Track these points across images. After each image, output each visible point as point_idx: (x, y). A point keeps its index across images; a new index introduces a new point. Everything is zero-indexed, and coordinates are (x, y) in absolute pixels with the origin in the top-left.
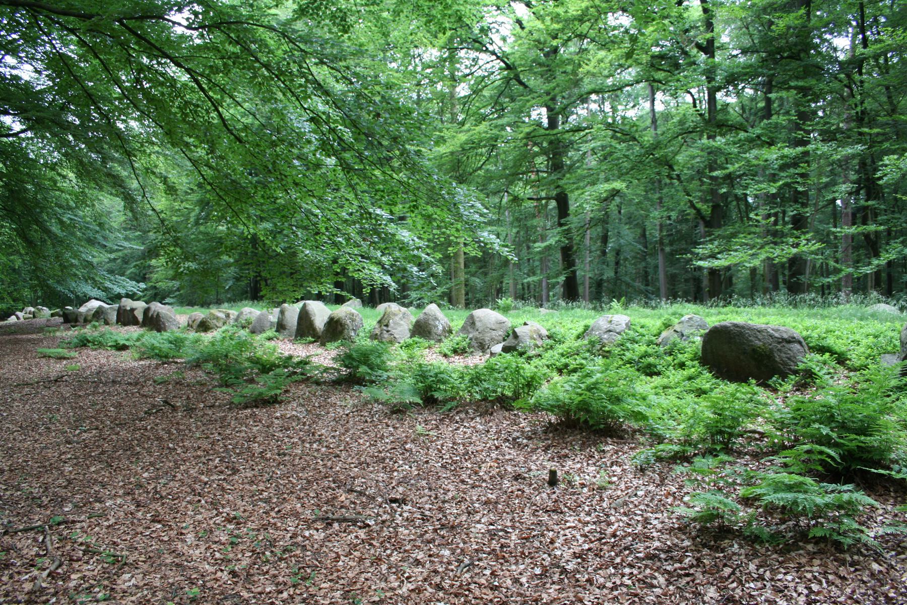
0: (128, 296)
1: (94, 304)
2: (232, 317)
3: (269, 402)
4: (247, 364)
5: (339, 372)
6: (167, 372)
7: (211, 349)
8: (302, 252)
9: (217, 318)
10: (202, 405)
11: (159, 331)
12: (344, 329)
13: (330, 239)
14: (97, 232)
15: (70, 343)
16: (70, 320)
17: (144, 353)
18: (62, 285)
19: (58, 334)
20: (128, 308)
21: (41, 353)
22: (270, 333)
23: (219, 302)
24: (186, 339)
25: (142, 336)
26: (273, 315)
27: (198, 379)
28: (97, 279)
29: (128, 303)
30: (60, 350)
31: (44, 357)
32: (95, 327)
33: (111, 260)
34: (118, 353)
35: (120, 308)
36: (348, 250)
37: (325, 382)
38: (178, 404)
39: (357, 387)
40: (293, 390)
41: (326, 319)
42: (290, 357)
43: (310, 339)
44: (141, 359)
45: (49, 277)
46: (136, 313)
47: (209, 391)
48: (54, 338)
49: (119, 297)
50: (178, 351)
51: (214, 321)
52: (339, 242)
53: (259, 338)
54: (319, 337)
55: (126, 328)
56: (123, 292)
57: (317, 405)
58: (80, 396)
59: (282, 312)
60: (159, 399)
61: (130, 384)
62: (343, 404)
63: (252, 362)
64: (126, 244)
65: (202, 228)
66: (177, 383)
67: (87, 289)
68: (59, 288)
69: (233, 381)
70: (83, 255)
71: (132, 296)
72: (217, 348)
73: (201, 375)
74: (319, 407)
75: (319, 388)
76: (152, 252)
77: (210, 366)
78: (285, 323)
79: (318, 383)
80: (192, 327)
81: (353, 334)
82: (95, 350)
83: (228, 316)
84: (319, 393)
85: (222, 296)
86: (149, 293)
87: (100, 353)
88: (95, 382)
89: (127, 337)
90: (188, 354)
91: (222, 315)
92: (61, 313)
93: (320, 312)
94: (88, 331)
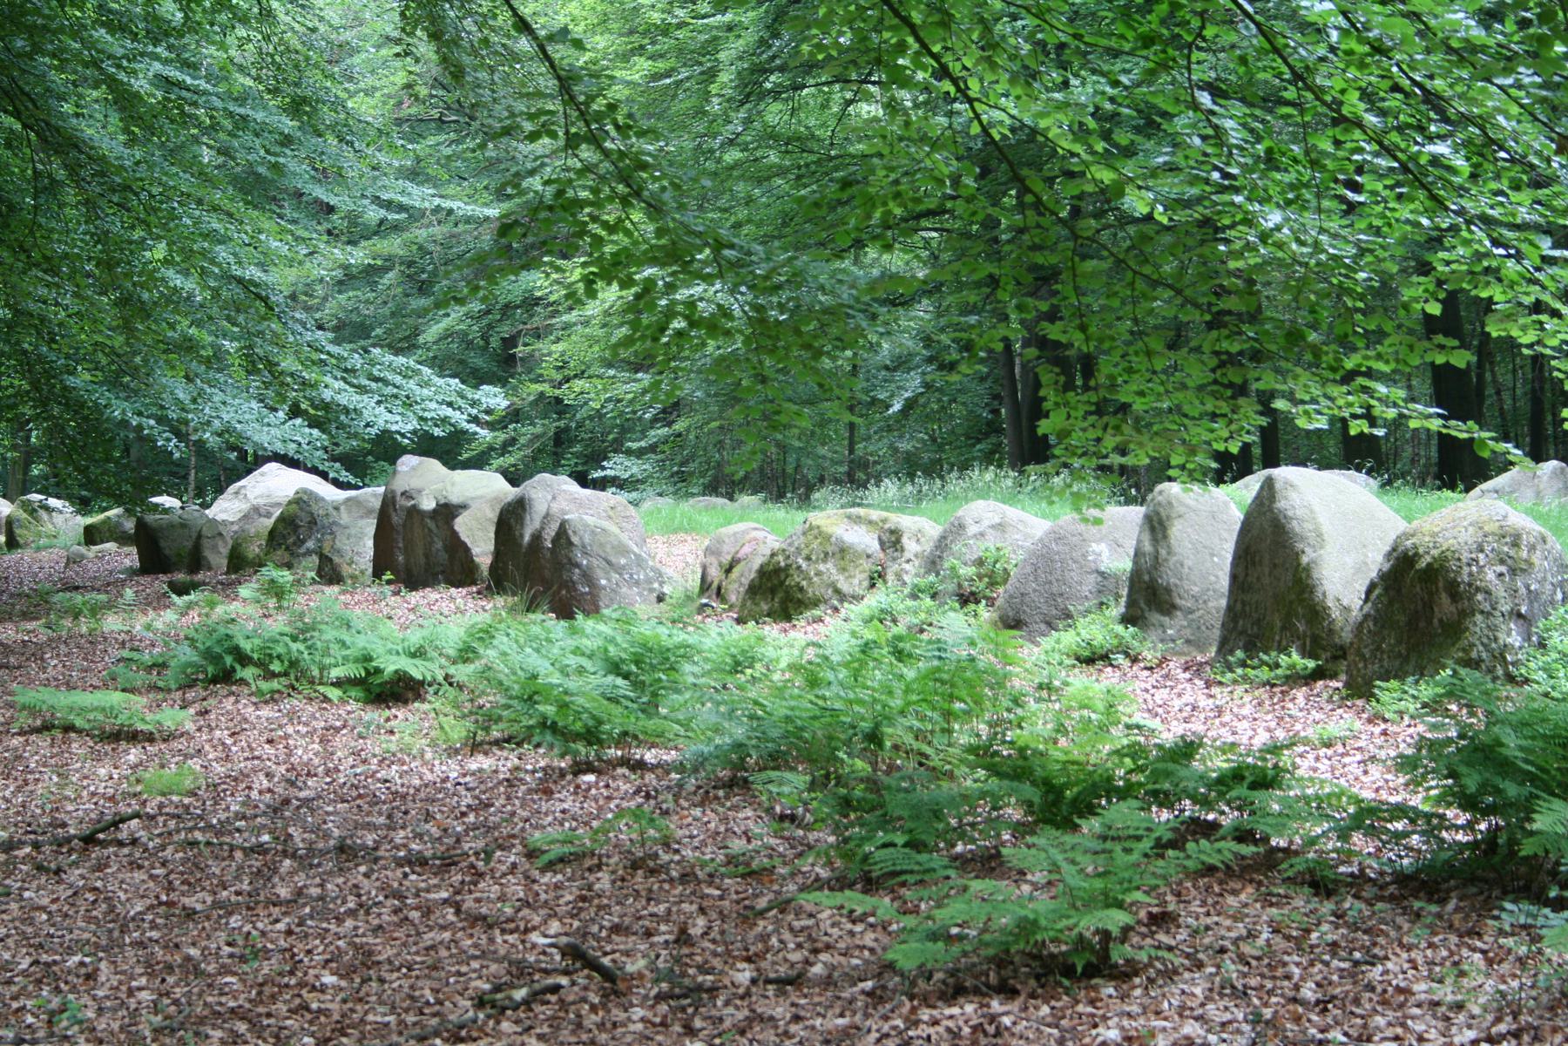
0: (427, 446)
1: (275, 485)
2: (911, 546)
3: (1069, 971)
4: (973, 780)
5: (1429, 833)
6: (596, 809)
7: (805, 704)
8: (1249, 222)
9: (843, 553)
10: (744, 975)
11: (565, 611)
12: (1466, 614)
13: (1388, 151)
14: (287, 141)
15: (161, 666)
16: (169, 558)
17: (491, 719)
18: (131, 394)
19: (112, 623)
20: (428, 504)
21: (33, 711)
22: (1100, 628)
23: (857, 476)
24: (687, 652)
25: (486, 634)
26: (1111, 537)
27: (738, 845)
28: (288, 363)
29: (426, 480)
30: (116, 698)
31: (46, 727)
32: (276, 591)
33: (349, 278)
34: (374, 715)
35: (388, 502)
36: (1479, 203)
37: (1360, 879)
38: (635, 966)
39: (1514, 912)
40: (1193, 913)
41: (1376, 561)
42: (1186, 750)
43: (1296, 659)
44: (475, 747)
45: (76, 358)
46: (462, 525)
47: (784, 906)
48: (95, 639)
49: (387, 449)
50: (649, 709)
51: (829, 567)
52: (1435, 161)
53: (1033, 657)
54: (1340, 653)
55: (415, 597)
56: (403, 425)
57: (1309, 992)
58: (190, 914)
59: (1156, 526)
60: (546, 936)
61: (418, 862)
62: (1446, 993)
63: (994, 770)
64: (419, 196)
65: (774, 113)
66: (635, 865)
67: (240, 412)
68: (119, 409)
69: (897, 857)
70: (222, 253)
71: (448, 448)
72: (833, 695)
73: (749, 828)
74: (1322, 1006)
75: (1328, 907)
76: (532, 234)
77: (791, 785)
78: (1167, 577)
79: (1321, 884)
80: (719, 594)
81: (1515, 639)
82: (273, 698)
83: (892, 541)
84: (1325, 933)
85: (876, 448)
86: (527, 431)
87: (292, 716)
88: (260, 849)
89: (415, 638)
90: (694, 726)
91: (864, 539)
92: (129, 525)
93: (1349, 527)
94: (245, 613)
